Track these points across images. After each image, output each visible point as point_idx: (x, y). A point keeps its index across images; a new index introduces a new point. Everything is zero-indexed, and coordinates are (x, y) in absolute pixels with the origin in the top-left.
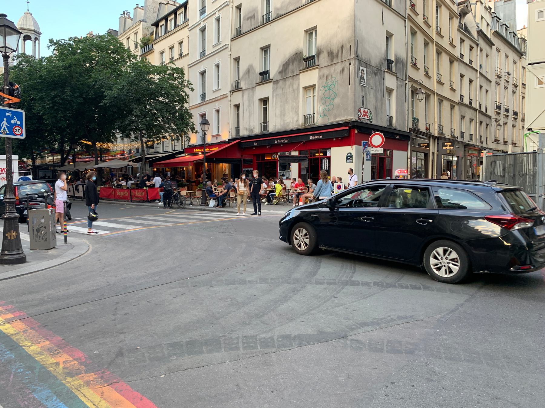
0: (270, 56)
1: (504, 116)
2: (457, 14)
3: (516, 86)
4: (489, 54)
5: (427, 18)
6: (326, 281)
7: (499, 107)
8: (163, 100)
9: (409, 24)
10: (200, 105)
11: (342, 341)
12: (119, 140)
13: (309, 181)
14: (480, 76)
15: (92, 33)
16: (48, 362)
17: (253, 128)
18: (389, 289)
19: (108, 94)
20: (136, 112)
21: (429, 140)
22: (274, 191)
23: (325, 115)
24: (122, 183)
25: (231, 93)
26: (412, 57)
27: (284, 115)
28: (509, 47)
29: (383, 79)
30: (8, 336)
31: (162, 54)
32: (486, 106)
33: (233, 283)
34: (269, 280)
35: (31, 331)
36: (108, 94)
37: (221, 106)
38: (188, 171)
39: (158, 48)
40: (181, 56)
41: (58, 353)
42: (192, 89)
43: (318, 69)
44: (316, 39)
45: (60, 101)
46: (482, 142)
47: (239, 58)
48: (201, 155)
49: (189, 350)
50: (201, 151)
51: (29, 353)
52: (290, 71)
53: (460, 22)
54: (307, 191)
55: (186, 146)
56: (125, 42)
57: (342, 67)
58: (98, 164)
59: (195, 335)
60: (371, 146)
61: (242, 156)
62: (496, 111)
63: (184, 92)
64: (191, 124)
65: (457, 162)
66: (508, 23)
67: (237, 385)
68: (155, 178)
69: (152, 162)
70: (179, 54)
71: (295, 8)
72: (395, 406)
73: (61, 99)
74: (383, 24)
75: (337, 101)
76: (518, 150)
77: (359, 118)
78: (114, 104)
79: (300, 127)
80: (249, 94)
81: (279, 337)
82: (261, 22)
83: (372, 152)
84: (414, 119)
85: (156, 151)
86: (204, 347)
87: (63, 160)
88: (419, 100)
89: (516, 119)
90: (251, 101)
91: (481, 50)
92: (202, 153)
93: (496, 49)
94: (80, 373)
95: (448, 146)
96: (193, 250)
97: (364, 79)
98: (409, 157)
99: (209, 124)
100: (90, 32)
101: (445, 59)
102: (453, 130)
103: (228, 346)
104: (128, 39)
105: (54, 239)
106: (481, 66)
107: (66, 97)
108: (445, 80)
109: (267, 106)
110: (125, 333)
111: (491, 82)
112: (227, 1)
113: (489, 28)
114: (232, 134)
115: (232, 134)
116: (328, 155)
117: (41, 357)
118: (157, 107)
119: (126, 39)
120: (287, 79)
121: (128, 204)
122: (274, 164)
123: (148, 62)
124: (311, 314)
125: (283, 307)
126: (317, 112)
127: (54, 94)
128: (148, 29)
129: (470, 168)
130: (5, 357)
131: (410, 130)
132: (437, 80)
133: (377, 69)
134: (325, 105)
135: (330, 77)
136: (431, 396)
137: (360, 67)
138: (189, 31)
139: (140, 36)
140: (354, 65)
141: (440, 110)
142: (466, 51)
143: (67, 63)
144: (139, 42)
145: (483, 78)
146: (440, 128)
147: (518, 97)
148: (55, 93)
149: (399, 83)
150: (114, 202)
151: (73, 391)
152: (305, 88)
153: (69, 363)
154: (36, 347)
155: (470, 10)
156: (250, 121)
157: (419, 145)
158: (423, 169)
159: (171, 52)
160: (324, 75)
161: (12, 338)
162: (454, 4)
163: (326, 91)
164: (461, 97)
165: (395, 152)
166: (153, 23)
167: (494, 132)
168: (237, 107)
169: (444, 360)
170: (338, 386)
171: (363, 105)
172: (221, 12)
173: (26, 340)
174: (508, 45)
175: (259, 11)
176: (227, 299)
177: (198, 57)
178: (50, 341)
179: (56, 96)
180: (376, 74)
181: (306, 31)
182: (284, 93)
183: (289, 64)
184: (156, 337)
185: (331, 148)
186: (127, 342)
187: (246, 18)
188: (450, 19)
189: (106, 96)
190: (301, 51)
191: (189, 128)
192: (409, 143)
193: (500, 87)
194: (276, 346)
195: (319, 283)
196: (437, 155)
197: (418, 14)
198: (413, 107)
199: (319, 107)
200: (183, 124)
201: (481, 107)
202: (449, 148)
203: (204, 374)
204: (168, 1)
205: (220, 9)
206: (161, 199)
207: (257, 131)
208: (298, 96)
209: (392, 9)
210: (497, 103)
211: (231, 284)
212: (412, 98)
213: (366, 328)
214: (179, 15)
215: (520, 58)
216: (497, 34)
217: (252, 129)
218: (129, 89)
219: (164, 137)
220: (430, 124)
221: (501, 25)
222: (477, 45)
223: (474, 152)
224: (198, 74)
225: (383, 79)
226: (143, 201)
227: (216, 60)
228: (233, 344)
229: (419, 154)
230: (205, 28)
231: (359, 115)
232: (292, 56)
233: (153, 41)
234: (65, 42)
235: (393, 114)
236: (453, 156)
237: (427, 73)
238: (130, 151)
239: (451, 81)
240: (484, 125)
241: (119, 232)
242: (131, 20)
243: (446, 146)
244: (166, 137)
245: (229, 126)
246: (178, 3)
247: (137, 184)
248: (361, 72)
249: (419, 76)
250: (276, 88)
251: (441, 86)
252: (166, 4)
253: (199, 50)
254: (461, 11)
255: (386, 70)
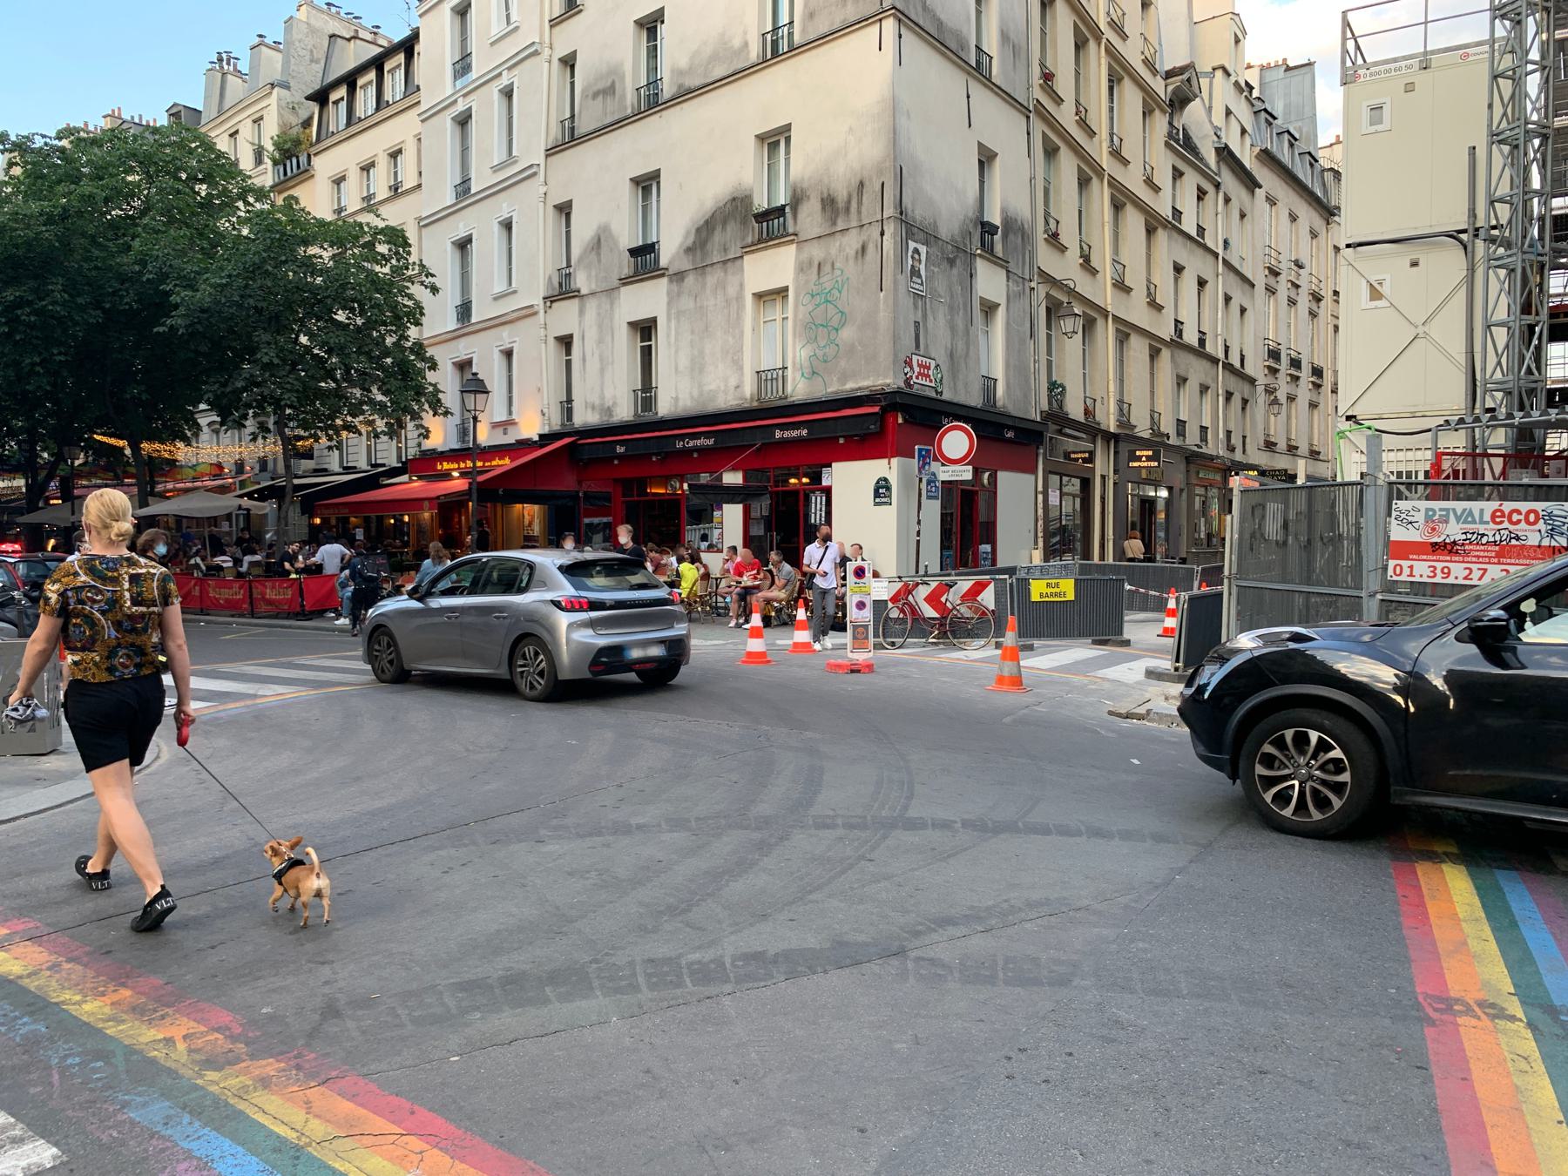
0: (658, 201)
1: (1289, 379)
2: (1165, 102)
3: (1317, 298)
4: (1247, 211)
5: (1086, 111)
6: (839, 821)
7: (1274, 355)
8: (349, 318)
9: (1038, 127)
10: (454, 336)
11: (895, 962)
12: (206, 434)
13: (773, 556)
14: (1226, 269)
15: (119, 114)
16: (143, 1039)
17: (611, 404)
18: (1003, 836)
19: (183, 298)
20: (267, 355)
21: (1094, 442)
22: (677, 583)
23: (814, 373)
24: (223, 561)
25: (548, 304)
26: (1047, 215)
27: (701, 370)
28: (1298, 193)
29: (971, 276)
30: (10, 982)
31: (338, 184)
32: (1241, 351)
33: (597, 831)
34: (693, 823)
35: (69, 966)
36: (183, 298)
37: (517, 339)
38: (419, 525)
39: (325, 165)
40: (396, 191)
41: (163, 1017)
42: (434, 290)
43: (795, 245)
44: (787, 160)
45: (33, 319)
46: (1232, 449)
47: (569, 204)
48: (458, 478)
49: (510, 997)
50: (459, 468)
51: (84, 1018)
52: (716, 246)
53: (1170, 124)
54: (768, 582)
55: (412, 453)
56: (223, 144)
57: (861, 243)
58: (147, 505)
59: (518, 961)
60: (938, 460)
61: (580, 483)
62: (1267, 363)
63: (410, 297)
64: (431, 389)
65: (1168, 502)
66: (1295, 128)
67: (648, 1072)
68: (322, 548)
69: (312, 500)
70: (390, 187)
71: (730, 72)
72: (1032, 1099)
73: (36, 312)
74: (970, 126)
75: (847, 334)
76: (1323, 470)
77: (907, 382)
78: (201, 330)
79: (746, 405)
80: (599, 307)
81: (734, 959)
82: (633, 105)
83: (943, 477)
84: (1053, 386)
85: (318, 467)
86: (548, 989)
87: (36, 494)
88: (1065, 334)
89: (1317, 386)
90: (604, 326)
91: (1227, 200)
92: (463, 475)
93: (1264, 199)
94: (237, 1060)
95: (1144, 459)
96: (467, 750)
97: (919, 276)
98: (1040, 488)
99: (487, 392)
100: (113, 111)
101: (1134, 221)
102: (1156, 415)
103: (611, 985)
104: (233, 135)
105: (56, 724)
106: (1226, 243)
107: (50, 308)
108: (1135, 279)
109: (653, 343)
110: (333, 962)
111: (1253, 286)
112: (533, 43)
113: (1248, 141)
114: (549, 419)
115: (549, 419)
116: (825, 483)
117: (120, 1028)
118: (332, 341)
119: (226, 136)
120: (709, 269)
121: (243, 624)
122: (672, 505)
123: (303, 210)
124: (811, 902)
125: (737, 888)
126: (794, 363)
127: (12, 298)
128: (293, 108)
129: (1203, 520)
130: (21, 1032)
131: (1044, 415)
132: (1113, 279)
133: (955, 250)
134: (815, 345)
135: (827, 268)
136: (1112, 1074)
137: (910, 242)
138: (422, 121)
139: (271, 129)
140: (894, 235)
141: (1122, 361)
142: (1188, 204)
143: (54, 206)
144: (269, 146)
145: (1232, 275)
146: (1121, 410)
147: (1322, 325)
148: (17, 294)
149: (1014, 288)
150: (198, 617)
151: (231, 1101)
152: (759, 296)
153: (199, 1038)
154: (97, 1003)
155: (1197, 92)
156: (602, 384)
157: (1067, 455)
158: (1078, 522)
159: (365, 179)
160: (810, 263)
161: (23, 984)
162: (1155, 75)
163: (818, 305)
164: (1176, 326)
165: (1003, 476)
166: (310, 91)
167: (1262, 421)
168: (566, 342)
169: (1142, 995)
170: (893, 1063)
171: (918, 346)
172: (516, 71)
173: (63, 988)
174: (1296, 188)
175: (627, 74)
176: (588, 872)
177: (449, 199)
178: (133, 988)
179: (20, 303)
180: (952, 262)
181: (761, 138)
182: (701, 307)
183: (714, 229)
184: (418, 969)
185: (833, 464)
186: (342, 984)
187: (590, 93)
188: (1144, 113)
189: (176, 307)
190: (747, 193)
191: (423, 400)
192: (1042, 451)
193: (1276, 301)
194: (732, 979)
195: (824, 824)
196: (1115, 484)
197: (1063, 101)
198: (1049, 353)
199: (798, 350)
200: (406, 388)
201: (1230, 353)
202: (1146, 464)
203: (559, 1049)
204: (357, 31)
205: (515, 63)
206: (346, 609)
207: (624, 412)
208: (739, 318)
209: (994, 84)
210: (1271, 343)
211: (590, 835)
212: (1049, 326)
213: (952, 931)
214: (388, 72)
215: (1328, 223)
216: (1267, 157)
217: (609, 408)
218: (246, 286)
219: (349, 428)
220: (1095, 400)
221: (1278, 134)
222: (1217, 186)
223: (1211, 476)
224: (449, 247)
225: (971, 276)
226: (290, 615)
227: (503, 206)
228: (621, 978)
229: (1065, 479)
230: (470, 116)
231: (906, 374)
232: (721, 204)
233: (312, 145)
234: (46, 144)
235: (999, 372)
236: (1157, 485)
237: (1086, 259)
238: (240, 467)
239: (1149, 281)
240: (1236, 401)
241: (238, 705)
242: (240, 81)
243: (1139, 459)
244: (355, 427)
245: (543, 397)
246: (385, 37)
247: (268, 564)
248: (912, 257)
249: (1065, 267)
250: (679, 294)
251: (1124, 295)
252: (349, 40)
253: (452, 177)
254: (1174, 92)
255: (979, 252)
